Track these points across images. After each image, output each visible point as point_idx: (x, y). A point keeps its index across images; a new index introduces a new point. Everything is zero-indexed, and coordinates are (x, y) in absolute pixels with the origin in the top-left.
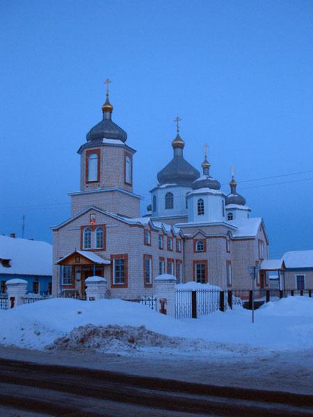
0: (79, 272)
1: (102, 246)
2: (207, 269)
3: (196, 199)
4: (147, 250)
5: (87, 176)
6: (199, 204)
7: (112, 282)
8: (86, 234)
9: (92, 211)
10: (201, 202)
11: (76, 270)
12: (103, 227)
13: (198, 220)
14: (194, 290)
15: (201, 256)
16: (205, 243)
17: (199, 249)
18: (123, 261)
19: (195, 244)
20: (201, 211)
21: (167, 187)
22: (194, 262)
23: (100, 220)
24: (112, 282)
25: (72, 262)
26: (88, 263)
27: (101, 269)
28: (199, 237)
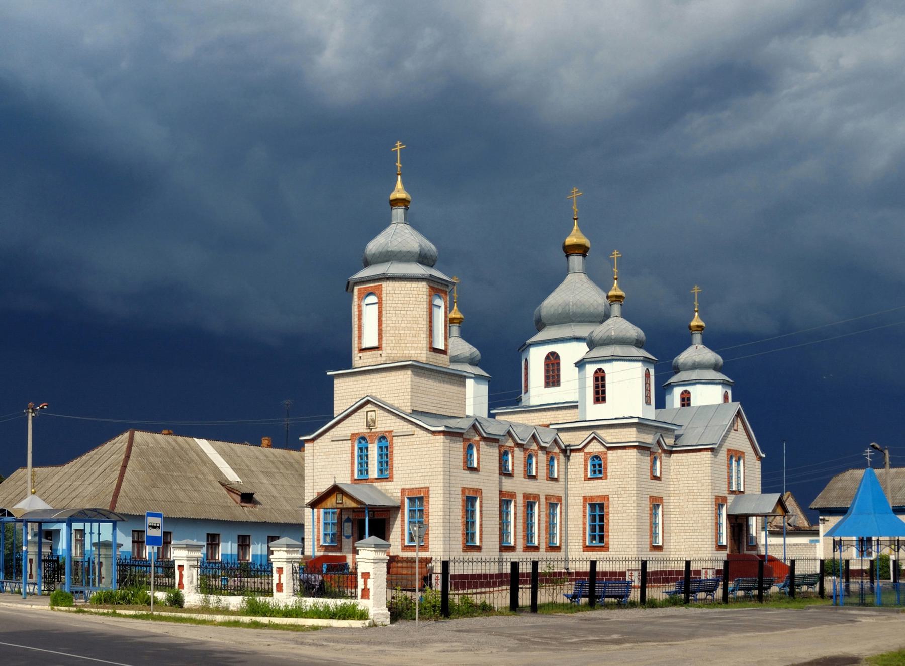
0: (348, 520)
1: (386, 472)
2: (608, 514)
3: (591, 369)
4: (471, 481)
5: (380, 312)
6: (596, 379)
7: (403, 540)
8: (361, 449)
9: (369, 405)
10: (600, 375)
11: (345, 517)
12: (384, 440)
13: (594, 412)
14: (688, 559)
15: (597, 488)
16: (606, 459)
17: (595, 472)
18: (421, 499)
19: (586, 461)
20: (600, 396)
21: (66, 611)
22: (585, 498)
23: (385, 423)
24: (403, 540)
25: (331, 502)
26: (354, 505)
27: (32, 568)
28: (595, 448)
